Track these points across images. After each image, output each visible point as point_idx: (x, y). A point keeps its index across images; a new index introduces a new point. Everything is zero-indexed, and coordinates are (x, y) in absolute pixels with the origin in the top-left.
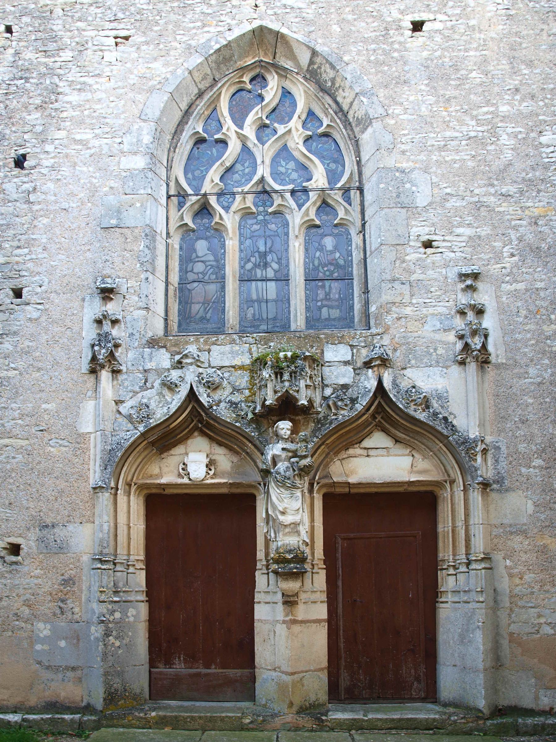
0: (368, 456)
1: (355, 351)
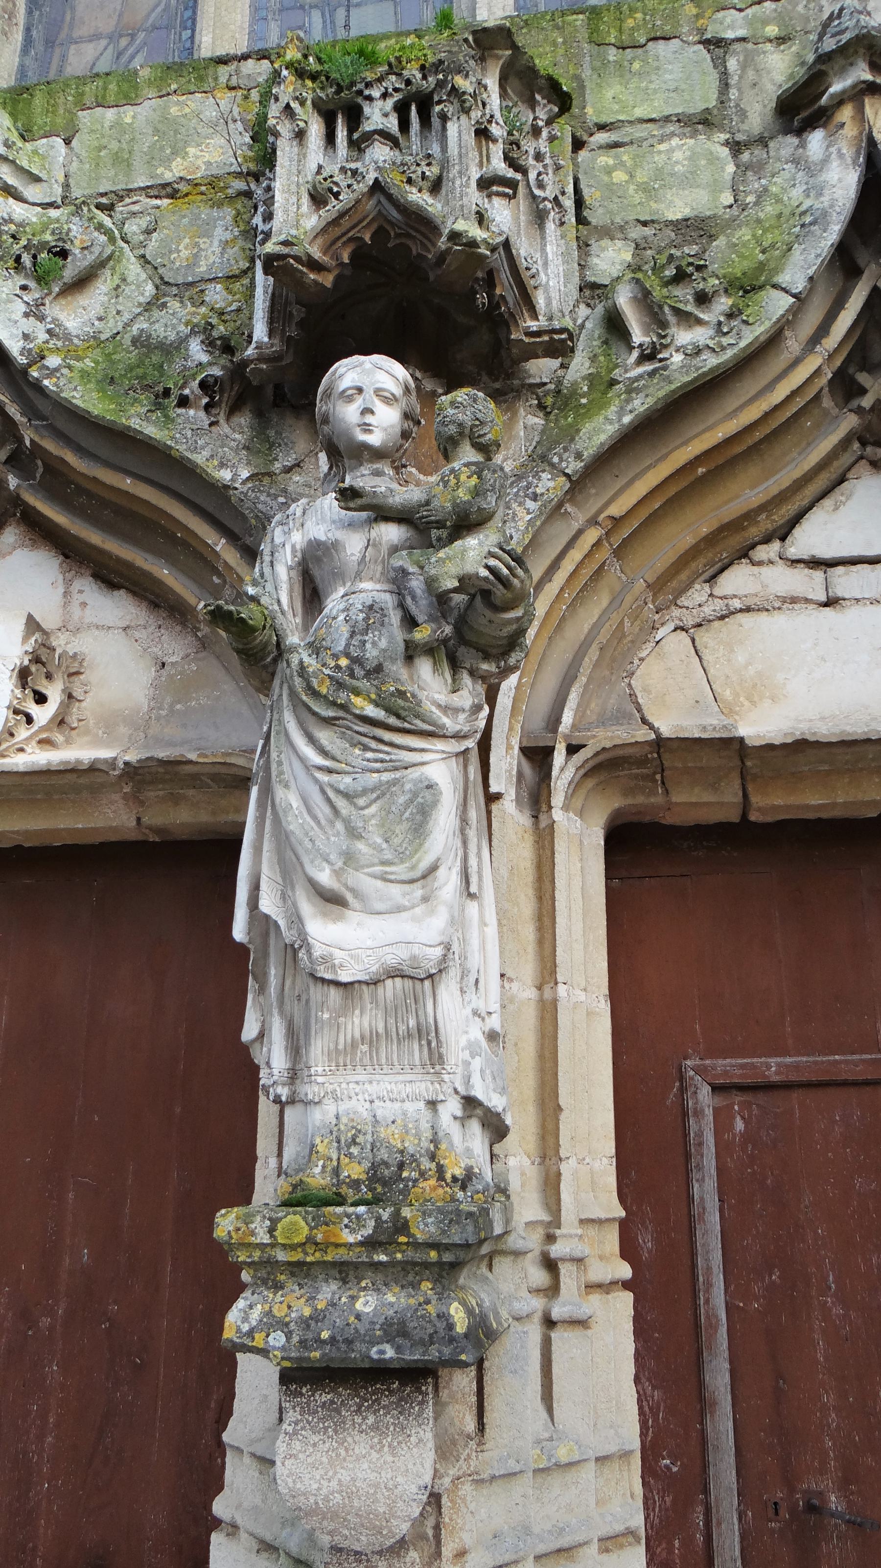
0: (831, 602)
1: (732, 64)
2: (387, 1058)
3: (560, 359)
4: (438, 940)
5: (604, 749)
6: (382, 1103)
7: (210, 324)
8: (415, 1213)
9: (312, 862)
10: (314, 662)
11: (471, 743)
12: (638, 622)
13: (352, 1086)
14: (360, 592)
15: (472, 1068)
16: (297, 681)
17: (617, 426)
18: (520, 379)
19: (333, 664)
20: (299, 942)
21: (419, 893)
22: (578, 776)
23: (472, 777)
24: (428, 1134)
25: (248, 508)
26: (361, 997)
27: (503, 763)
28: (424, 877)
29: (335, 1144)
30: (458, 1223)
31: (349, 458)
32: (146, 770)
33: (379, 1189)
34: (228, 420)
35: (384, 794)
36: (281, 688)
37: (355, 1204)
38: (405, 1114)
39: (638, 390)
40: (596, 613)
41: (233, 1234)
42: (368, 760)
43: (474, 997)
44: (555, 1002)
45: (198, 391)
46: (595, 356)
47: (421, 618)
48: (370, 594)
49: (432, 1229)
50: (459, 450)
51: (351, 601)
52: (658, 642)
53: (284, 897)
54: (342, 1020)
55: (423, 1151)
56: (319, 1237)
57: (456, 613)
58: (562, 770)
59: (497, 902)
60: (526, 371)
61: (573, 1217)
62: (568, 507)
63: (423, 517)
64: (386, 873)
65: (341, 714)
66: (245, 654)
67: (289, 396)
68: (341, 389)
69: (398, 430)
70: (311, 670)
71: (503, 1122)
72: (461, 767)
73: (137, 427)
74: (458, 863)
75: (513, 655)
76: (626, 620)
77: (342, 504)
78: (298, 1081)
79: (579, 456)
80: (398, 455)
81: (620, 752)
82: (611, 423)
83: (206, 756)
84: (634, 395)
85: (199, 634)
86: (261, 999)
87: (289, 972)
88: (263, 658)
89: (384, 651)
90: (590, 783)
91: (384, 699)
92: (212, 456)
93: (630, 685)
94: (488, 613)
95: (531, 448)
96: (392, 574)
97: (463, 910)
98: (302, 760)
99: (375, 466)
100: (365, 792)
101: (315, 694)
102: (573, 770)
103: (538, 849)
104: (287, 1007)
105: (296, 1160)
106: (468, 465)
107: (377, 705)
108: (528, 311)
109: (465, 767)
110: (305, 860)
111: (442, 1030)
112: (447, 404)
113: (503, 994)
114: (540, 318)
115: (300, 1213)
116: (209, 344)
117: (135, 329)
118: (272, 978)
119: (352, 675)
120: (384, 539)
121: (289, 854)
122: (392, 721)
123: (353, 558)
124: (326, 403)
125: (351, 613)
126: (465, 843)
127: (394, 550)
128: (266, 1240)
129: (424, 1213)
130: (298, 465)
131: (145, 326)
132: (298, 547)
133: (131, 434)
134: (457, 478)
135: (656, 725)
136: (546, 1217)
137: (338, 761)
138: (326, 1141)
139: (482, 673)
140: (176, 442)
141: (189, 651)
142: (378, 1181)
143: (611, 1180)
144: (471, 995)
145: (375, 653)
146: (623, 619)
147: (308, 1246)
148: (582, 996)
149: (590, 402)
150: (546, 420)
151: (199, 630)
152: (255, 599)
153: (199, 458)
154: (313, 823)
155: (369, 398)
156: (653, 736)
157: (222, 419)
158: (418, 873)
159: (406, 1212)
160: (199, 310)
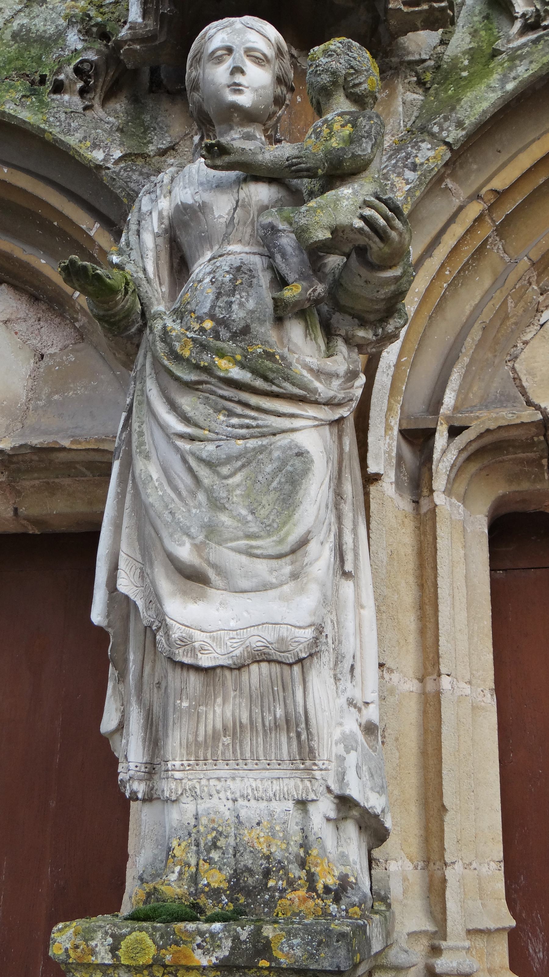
2: (252, 752)
3: (441, 31)
4: (308, 620)
5: (488, 431)
6: (246, 803)
7: (88, 16)
8: (278, 932)
9: (171, 536)
10: (178, 327)
11: (345, 412)
12: (522, 304)
13: (212, 782)
14: (228, 254)
15: (347, 764)
16: (160, 346)
17: (500, 94)
18: (398, 56)
19: (197, 327)
20: (157, 623)
21: (287, 570)
22: (461, 459)
23: (347, 448)
24: (297, 838)
25: (120, 187)
26: (223, 684)
27: (382, 443)
28: (293, 551)
29: (194, 848)
30: (328, 946)
32: (20, 458)
33: (242, 900)
34: (103, 105)
35: (249, 463)
37: (211, 920)
38: (271, 815)
39: (522, 58)
40: (478, 295)
41: (71, 952)
43: (349, 685)
44: (438, 694)
45: (73, 76)
46: (476, 31)
47: (291, 277)
48: (239, 257)
49: (298, 952)
51: (218, 264)
52: (542, 326)
53: (142, 576)
54: (203, 708)
55: (291, 857)
56: (168, 959)
58: (444, 452)
59: (375, 587)
60: (404, 49)
61: (460, 928)
62: (449, 183)
64: (252, 547)
66: (107, 322)
67: (165, 82)
68: (211, 50)
69: (270, 92)
70: (174, 333)
71: (382, 824)
72: (335, 438)
73: (11, 112)
74: (332, 538)
75: (391, 321)
76: (510, 300)
77: (209, 162)
78: (156, 777)
79: (460, 124)
81: (504, 435)
82: (493, 91)
83: (80, 443)
84: (517, 62)
85: (77, 325)
86: (121, 687)
87: (149, 657)
88: (127, 328)
89: (252, 312)
90: (473, 468)
91: (250, 360)
92: (85, 138)
93: (513, 369)
94: (364, 272)
96: (261, 232)
97: (337, 589)
98: (163, 427)
99: (246, 130)
100: (229, 460)
101: (177, 358)
102: (455, 452)
103: (419, 535)
104: (146, 696)
105: (152, 864)
106: (341, 114)
107: (243, 366)
109: (340, 438)
110: (164, 534)
111: (313, 721)
112: (319, 54)
113: (381, 687)
115: (146, 930)
116: (86, 32)
117: (15, 26)
118: (131, 664)
119: (217, 337)
120: (254, 199)
121: (149, 529)
122: (259, 383)
123: (221, 220)
124: (196, 68)
125: (217, 275)
126: (339, 518)
127: (264, 209)
128: (108, 960)
129: (289, 933)
131: (25, 21)
132: (165, 213)
133: (6, 120)
134: (330, 127)
135: (543, 406)
136: (430, 927)
137: (201, 428)
138: (184, 844)
140: (50, 126)
141: (67, 342)
142: (241, 890)
143: (500, 886)
144: (346, 683)
145: (242, 314)
146: (506, 300)
147: (155, 968)
148: (467, 689)
149: (471, 74)
150: (425, 96)
151: (77, 320)
152: (120, 267)
153: (72, 140)
154: (173, 495)
155: (239, 56)
156: (540, 417)
157: (97, 103)
158: (286, 548)
159: (268, 931)
160: (78, 4)
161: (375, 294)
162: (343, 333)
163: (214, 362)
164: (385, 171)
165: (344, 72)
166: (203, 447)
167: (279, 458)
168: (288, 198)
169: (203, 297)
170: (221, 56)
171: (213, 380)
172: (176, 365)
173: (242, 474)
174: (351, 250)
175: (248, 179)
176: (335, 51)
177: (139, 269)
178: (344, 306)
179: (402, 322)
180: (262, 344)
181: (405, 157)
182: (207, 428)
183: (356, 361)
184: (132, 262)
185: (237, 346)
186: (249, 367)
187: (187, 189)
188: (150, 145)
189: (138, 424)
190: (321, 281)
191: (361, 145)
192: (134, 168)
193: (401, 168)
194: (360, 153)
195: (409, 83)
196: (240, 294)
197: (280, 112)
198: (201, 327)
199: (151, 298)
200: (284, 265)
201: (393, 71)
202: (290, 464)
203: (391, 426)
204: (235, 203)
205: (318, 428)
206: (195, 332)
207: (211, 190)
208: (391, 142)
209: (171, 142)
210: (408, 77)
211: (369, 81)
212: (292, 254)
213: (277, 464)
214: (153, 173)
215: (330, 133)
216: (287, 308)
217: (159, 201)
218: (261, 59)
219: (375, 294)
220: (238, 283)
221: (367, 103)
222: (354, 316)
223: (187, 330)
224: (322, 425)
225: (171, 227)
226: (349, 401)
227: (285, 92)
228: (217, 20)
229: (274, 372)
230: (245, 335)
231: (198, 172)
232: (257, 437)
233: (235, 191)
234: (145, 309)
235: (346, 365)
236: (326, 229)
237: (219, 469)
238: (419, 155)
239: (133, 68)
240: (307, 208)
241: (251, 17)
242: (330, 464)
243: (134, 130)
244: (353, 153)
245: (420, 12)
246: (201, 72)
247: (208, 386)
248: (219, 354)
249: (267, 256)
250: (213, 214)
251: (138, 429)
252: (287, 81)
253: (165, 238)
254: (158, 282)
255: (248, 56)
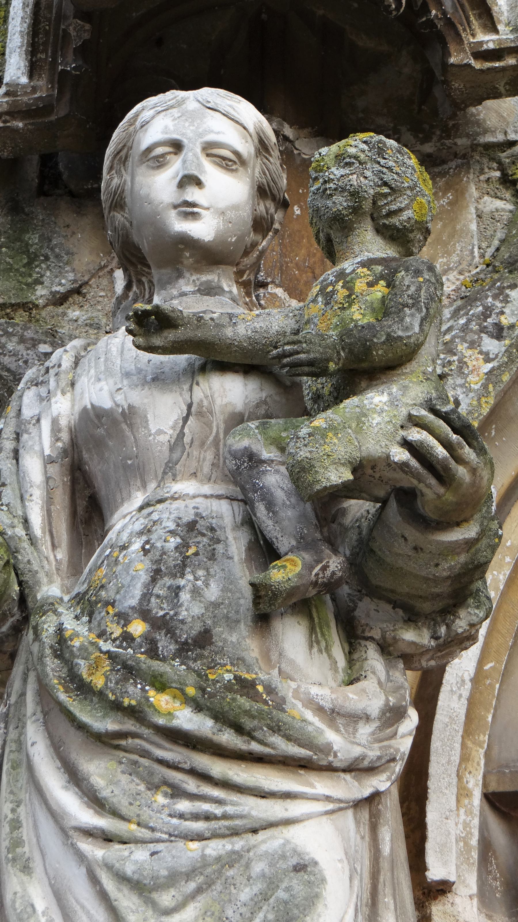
10: (83, 630)
14: (173, 498)
18: (468, 136)
19: (117, 632)
23: (386, 849)
27: (451, 823)
31: (160, 267)
35: (209, 884)
36: (25, 680)
42: (181, 816)
48: (192, 503)
50: (354, 239)
51: (155, 516)
57: (353, 536)
60: (478, 123)
63: (285, 355)
65: (130, 725)
67: (65, 177)
68: (144, 145)
70: (76, 643)
72: (365, 830)
75: (462, 613)
77: (141, 340)
80: (248, 261)
89: (216, 605)
91: (212, 696)
95: (490, 251)
96: (231, 464)
99: (204, 278)
106: (368, 264)
107: (198, 708)
108: (479, 17)
109: (374, 828)
112: (329, 160)
114: (500, 27)
120: (219, 402)
124: (119, 173)
125: (154, 537)
130: (77, 291)
132: (63, 422)
134: (349, 286)
139: (403, 648)
145: (197, 609)
161: (433, 570)
162: (376, 634)
163: (147, 699)
164: (448, 337)
165: (372, 192)
166: (126, 853)
167: (264, 875)
168: (277, 398)
169: (129, 579)
170: (163, 155)
171: (145, 731)
172: (80, 701)
173: (198, 905)
174: (390, 494)
175: (209, 366)
176: (356, 157)
177: (16, 521)
178: (377, 587)
179: (481, 615)
180: (232, 664)
181: (483, 314)
182: (135, 819)
183: (401, 687)
184: (4, 508)
185: (189, 668)
186: (209, 709)
187: (103, 383)
188: (39, 287)
189: (11, 806)
190: (335, 551)
191: (402, 320)
192: (10, 330)
193: (475, 333)
194: (400, 333)
195: (488, 180)
196: (193, 573)
197: (264, 243)
198: (126, 632)
199: (37, 572)
200: (270, 523)
201: (459, 161)
202: (284, 885)
203: (468, 790)
204: (185, 408)
205: (334, 816)
206: (114, 641)
207: (143, 385)
208: (458, 283)
209: (75, 281)
210: (486, 170)
211: (415, 206)
212: (284, 504)
213: (259, 886)
214: (44, 338)
215: (349, 296)
216: (276, 599)
217: (53, 400)
218: (230, 160)
219: (433, 570)
220: (191, 551)
221: (412, 241)
222: (395, 605)
223: (99, 636)
224: (340, 809)
225: (73, 446)
226: (389, 761)
227: (272, 210)
228: (155, 93)
229: (253, 717)
230: (203, 647)
231: (122, 352)
232: (223, 836)
233: (186, 387)
234: (27, 591)
235: (383, 698)
236: (343, 465)
237: (155, 896)
238: (506, 310)
239: (11, 156)
240: (310, 430)
241: (213, 90)
242: (356, 882)
243: (10, 261)
244: (388, 335)
245: (503, 69)
246: (129, 179)
247: (137, 741)
248: (157, 685)
249: (242, 500)
250: (147, 427)
251: (10, 816)
252: (275, 192)
253: (62, 465)
254: (49, 543)
255: (208, 155)
